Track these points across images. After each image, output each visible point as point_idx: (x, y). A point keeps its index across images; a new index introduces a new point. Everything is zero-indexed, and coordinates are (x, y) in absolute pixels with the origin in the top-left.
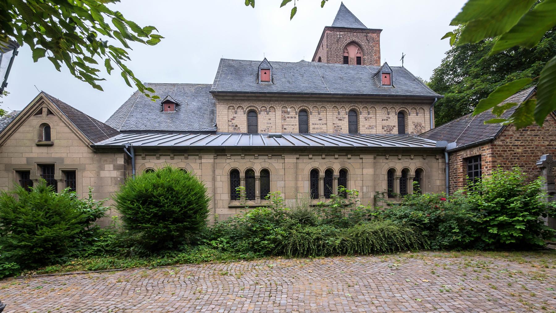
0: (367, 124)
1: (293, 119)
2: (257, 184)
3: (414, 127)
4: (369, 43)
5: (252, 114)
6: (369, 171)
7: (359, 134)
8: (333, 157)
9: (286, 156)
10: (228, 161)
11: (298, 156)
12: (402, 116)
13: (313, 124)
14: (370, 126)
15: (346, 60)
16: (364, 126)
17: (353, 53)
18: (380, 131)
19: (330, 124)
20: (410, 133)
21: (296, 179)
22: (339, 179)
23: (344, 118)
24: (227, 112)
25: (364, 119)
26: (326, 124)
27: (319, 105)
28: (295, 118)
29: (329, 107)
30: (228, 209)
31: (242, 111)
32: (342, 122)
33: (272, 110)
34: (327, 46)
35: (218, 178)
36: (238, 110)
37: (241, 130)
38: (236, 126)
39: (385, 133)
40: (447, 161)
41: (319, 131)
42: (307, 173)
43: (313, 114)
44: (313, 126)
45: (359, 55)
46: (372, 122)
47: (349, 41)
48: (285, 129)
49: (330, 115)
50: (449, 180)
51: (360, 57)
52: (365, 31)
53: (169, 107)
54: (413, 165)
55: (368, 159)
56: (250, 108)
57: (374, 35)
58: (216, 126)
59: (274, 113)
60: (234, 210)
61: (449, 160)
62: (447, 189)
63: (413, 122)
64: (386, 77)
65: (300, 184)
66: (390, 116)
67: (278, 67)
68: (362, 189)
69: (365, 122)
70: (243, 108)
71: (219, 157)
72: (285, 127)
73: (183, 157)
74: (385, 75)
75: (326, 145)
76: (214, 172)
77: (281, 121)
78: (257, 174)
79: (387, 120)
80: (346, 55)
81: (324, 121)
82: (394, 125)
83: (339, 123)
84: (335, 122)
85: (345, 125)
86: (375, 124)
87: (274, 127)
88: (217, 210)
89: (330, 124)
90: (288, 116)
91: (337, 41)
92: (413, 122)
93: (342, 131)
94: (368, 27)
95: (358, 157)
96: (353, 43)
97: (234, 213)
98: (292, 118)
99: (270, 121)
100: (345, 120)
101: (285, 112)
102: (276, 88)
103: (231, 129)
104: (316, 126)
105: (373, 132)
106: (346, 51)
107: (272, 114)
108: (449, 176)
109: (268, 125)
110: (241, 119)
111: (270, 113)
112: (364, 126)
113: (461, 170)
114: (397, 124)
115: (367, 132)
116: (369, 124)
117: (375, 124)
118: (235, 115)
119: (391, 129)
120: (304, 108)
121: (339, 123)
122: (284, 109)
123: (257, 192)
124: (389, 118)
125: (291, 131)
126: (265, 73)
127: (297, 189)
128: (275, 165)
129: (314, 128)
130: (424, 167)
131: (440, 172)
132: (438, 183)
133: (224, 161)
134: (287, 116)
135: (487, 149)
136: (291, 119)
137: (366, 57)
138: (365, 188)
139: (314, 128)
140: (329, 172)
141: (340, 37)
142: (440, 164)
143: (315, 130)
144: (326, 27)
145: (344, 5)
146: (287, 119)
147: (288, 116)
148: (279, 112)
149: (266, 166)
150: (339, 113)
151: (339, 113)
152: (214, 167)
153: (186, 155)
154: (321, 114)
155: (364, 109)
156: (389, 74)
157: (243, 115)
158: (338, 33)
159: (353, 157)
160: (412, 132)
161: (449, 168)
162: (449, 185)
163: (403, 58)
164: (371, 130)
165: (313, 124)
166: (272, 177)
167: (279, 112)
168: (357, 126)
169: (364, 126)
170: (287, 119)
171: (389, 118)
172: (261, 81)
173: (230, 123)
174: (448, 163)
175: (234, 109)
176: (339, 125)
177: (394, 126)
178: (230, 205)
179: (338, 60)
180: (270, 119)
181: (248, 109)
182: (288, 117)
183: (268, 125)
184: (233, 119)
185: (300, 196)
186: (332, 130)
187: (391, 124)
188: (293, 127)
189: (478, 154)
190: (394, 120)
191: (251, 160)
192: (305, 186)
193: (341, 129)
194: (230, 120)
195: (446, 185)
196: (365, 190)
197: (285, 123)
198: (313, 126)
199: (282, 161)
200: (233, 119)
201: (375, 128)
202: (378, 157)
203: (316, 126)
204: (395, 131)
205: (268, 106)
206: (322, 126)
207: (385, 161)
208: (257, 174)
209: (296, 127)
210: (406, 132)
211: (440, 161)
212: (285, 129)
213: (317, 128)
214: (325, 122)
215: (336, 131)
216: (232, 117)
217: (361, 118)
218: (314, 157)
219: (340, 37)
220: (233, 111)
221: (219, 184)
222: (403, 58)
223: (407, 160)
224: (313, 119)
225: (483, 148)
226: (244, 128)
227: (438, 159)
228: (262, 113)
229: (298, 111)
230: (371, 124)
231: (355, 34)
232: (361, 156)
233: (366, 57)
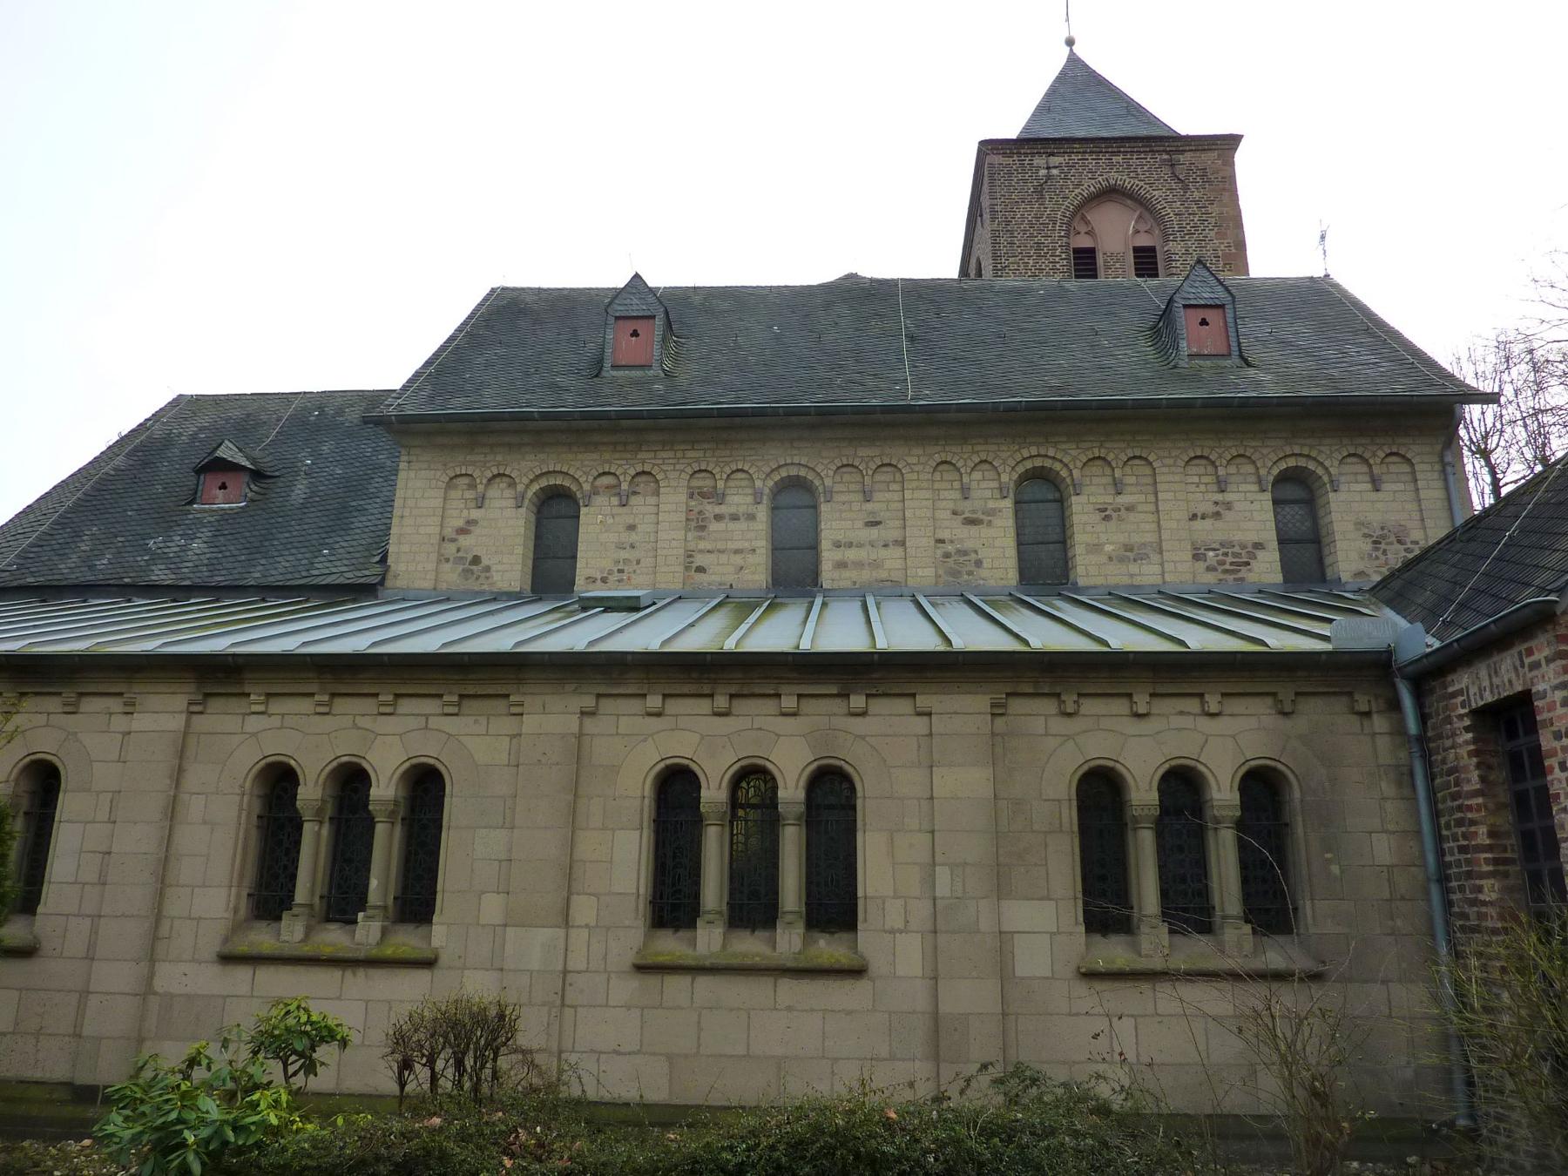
0: (1112, 537)
1: (742, 525)
2: (792, 843)
3: (1367, 546)
4: (1186, 189)
5: (1043, 499)
6: (965, 782)
7: (1077, 590)
8: (770, 705)
9: (528, 700)
10: (254, 723)
11: (589, 702)
12: (1298, 493)
13: (838, 545)
14: (1128, 548)
15: (1085, 262)
16: (1095, 547)
17: (1115, 232)
18: (1180, 571)
19: (920, 541)
20: (1345, 577)
21: (573, 819)
22: (1240, 825)
23: (992, 512)
24: (438, 503)
25: (1098, 516)
26: (903, 543)
27: (867, 454)
28: (751, 517)
29: (915, 460)
30: (216, 969)
31: (509, 493)
32: (983, 531)
33: (643, 484)
34: (993, 212)
35: (194, 807)
36: (493, 492)
37: (496, 577)
38: (476, 560)
39: (1210, 579)
40: (1412, 727)
41: (866, 575)
42: (634, 787)
43: (837, 498)
44: (838, 555)
45: (1144, 241)
46: (1139, 529)
47: (1089, 187)
48: (701, 570)
49: (918, 502)
50: (1439, 839)
51: (1152, 249)
52: (1165, 145)
53: (223, 487)
54: (789, 745)
55: (962, 712)
56: (544, 483)
57: (1208, 158)
58: (384, 560)
59: (652, 500)
60: (242, 973)
61: (1423, 718)
62: (1435, 890)
63: (1359, 524)
64: (1204, 322)
65: (589, 845)
66: (1229, 497)
67: (725, 306)
68: (930, 880)
69: (1101, 527)
70: (512, 485)
71: (215, 704)
72: (700, 560)
73: (53, 704)
74: (1201, 314)
75: (1036, 644)
76: (178, 775)
77: (681, 534)
78: (791, 791)
79: (1217, 515)
80: (1084, 242)
81: (890, 532)
82: (1252, 537)
83: (969, 537)
84: (945, 535)
85: (997, 551)
86: (1150, 538)
87: (647, 562)
88: (163, 969)
89: (920, 541)
90: (718, 510)
91: (1039, 191)
92: (1359, 524)
93: (984, 573)
94: (1183, 133)
95: (903, 705)
96: (1111, 193)
97: (244, 989)
98: (735, 518)
99: (634, 537)
100: (997, 522)
101: (703, 495)
102: (1265, 383)
103: (451, 577)
104: (851, 555)
105: (1148, 574)
106: (1083, 229)
107: (641, 505)
108: (1436, 814)
109: (623, 555)
110: (504, 534)
111: (634, 500)
112: (1095, 548)
113: (1473, 780)
114: (1270, 536)
115: (1116, 576)
116: (1122, 538)
117: (1150, 538)
118: (475, 514)
119: (1240, 558)
120: (793, 471)
121: (969, 537)
122: (703, 482)
123: (713, 889)
124: (1228, 506)
125: (730, 579)
126: (635, 334)
127: (569, 876)
128: (881, 743)
129: (841, 565)
130: (1291, 762)
131: (1388, 788)
132: (1384, 850)
133: (230, 723)
134: (711, 509)
135: (1549, 660)
136: (732, 526)
137: (1176, 247)
138: (943, 874)
139: (841, 565)
140: (351, 780)
141: (1049, 177)
142: (1383, 743)
143: (846, 574)
144: (983, 143)
145: (1079, 60)
146: (714, 526)
147: (718, 510)
148: (674, 498)
149: (428, 750)
150: (965, 493)
151: (965, 493)
152: (181, 754)
153: (69, 693)
154: (878, 496)
155: (1096, 469)
156: (1222, 306)
157: (510, 513)
158: (1038, 161)
159: (878, 705)
160: (1361, 574)
161: (1429, 765)
162: (1442, 866)
163: (1323, 237)
164: (1133, 568)
165: (838, 545)
166: (455, 808)
167: (674, 498)
168: (1065, 551)
169: (1095, 548)
170: (714, 526)
171: (1228, 506)
172: (615, 367)
173: (450, 549)
174: (1422, 739)
175: (472, 486)
176: (969, 545)
177: (1258, 546)
178: (227, 950)
179: (1044, 263)
180: (632, 528)
181: (536, 487)
182: (718, 518)
183: (623, 555)
184: (462, 531)
185: (584, 910)
186: (930, 572)
187: (1238, 536)
188: (738, 560)
189: (1519, 688)
190: (1253, 516)
191: (360, 721)
192: (623, 857)
193: (979, 563)
194: (449, 532)
195: (1424, 865)
196: (943, 886)
197: (702, 545)
198: (838, 555)
199: (506, 725)
200: (462, 531)
201: (1155, 557)
202: (1016, 705)
203: (851, 555)
204: (1267, 569)
205: (625, 469)
206: (883, 553)
207: (1060, 725)
208: (791, 791)
209: (751, 559)
210: (1329, 573)
211: (1380, 723)
212: (701, 570)
213: (859, 565)
214: (896, 534)
215: (955, 574)
216: (460, 523)
217: (1082, 510)
218: (674, 706)
219: (1049, 177)
220: (470, 494)
221: (190, 837)
222: (1323, 237)
223: (1186, 722)
224: (838, 525)
225: (1530, 652)
226: (511, 569)
227: (1368, 714)
228: (599, 500)
229: (766, 485)
230: (1136, 539)
231: (1120, 158)
232: (923, 701)
233: (1176, 247)
